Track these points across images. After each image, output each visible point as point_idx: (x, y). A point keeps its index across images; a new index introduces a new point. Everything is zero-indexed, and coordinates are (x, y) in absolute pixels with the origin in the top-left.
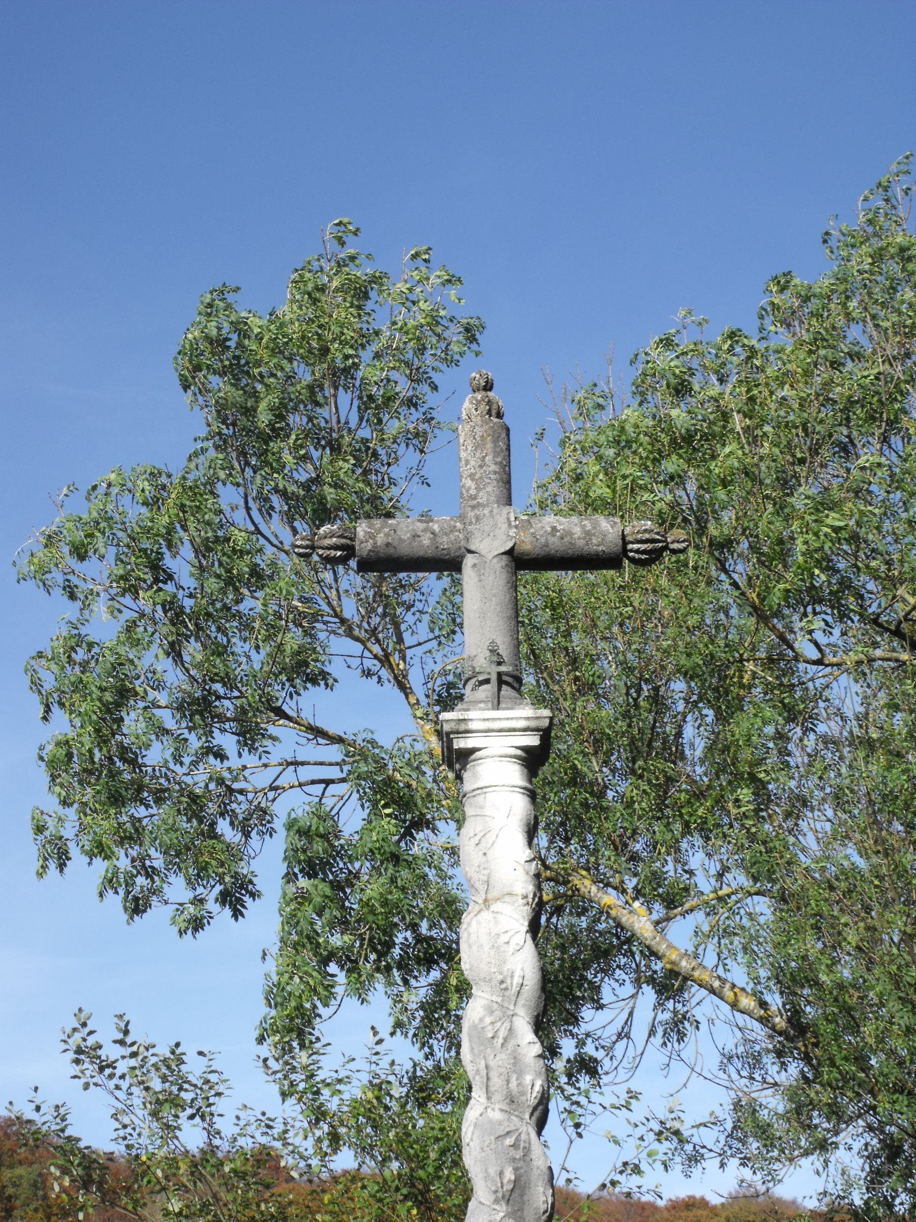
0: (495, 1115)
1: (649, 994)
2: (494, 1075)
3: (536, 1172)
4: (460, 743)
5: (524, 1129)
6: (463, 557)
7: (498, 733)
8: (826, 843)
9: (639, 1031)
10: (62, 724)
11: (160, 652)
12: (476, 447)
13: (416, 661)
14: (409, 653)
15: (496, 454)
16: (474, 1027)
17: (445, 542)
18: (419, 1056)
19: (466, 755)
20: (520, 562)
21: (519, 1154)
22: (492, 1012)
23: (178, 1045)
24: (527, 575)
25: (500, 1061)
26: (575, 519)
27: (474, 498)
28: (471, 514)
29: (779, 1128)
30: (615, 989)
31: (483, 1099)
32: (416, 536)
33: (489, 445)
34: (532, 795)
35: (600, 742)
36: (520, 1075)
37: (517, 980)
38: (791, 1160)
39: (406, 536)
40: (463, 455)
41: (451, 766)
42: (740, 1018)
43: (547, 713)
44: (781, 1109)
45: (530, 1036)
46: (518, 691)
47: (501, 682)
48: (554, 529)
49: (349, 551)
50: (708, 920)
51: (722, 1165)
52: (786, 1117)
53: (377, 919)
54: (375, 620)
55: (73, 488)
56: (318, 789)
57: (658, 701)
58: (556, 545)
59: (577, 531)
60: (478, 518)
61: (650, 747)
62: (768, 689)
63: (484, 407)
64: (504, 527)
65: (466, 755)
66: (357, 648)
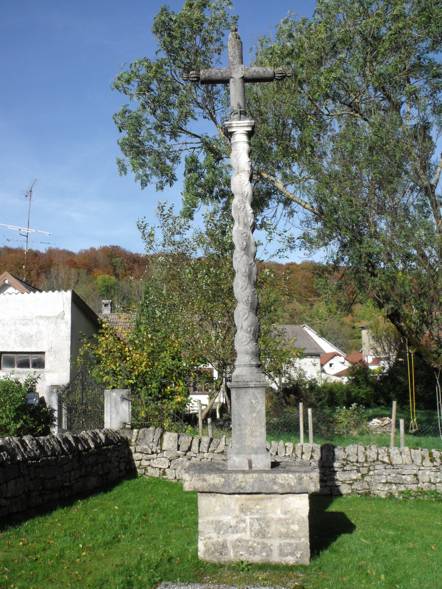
0: (241, 228)
1: (281, 205)
2: (240, 218)
3: (252, 243)
4: (230, 130)
5: (248, 232)
6: (229, 79)
7: (240, 128)
8: (329, 164)
9: (278, 215)
10: (125, 134)
11: (149, 114)
12: (233, 48)
13: (218, 114)
14: (216, 112)
15: (238, 50)
16: (235, 206)
17: (225, 75)
18: (223, 163)
19: (231, 134)
20: (245, 80)
21: (247, 238)
22: (240, 202)
23: (162, 208)
24: (247, 84)
25: (242, 214)
26: (260, 68)
27: (232, 62)
28: (232, 67)
29: (315, 240)
30: (273, 203)
31: (238, 224)
32: (217, 74)
33: (236, 47)
34: (250, 144)
35: (269, 136)
36: (247, 218)
37: (246, 193)
38: (318, 248)
39: (214, 74)
40: (229, 50)
41: (227, 137)
42: (306, 211)
43: (253, 121)
44: (316, 235)
45: (250, 208)
46: (245, 116)
47: (241, 113)
48: (255, 71)
49: (198, 78)
50: (298, 186)
51: (300, 250)
52: (317, 237)
53: (210, 185)
54: (207, 104)
55: (125, 64)
56: (192, 150)
57: (284, 125)
58: (255, 75)
59: (261, 71)
60: (234, 68)
61: (282, 137)
62: (315, 122)
63: (235, 36)
64: (241, 70)
65: (231, 134)
66: (201, 111)
